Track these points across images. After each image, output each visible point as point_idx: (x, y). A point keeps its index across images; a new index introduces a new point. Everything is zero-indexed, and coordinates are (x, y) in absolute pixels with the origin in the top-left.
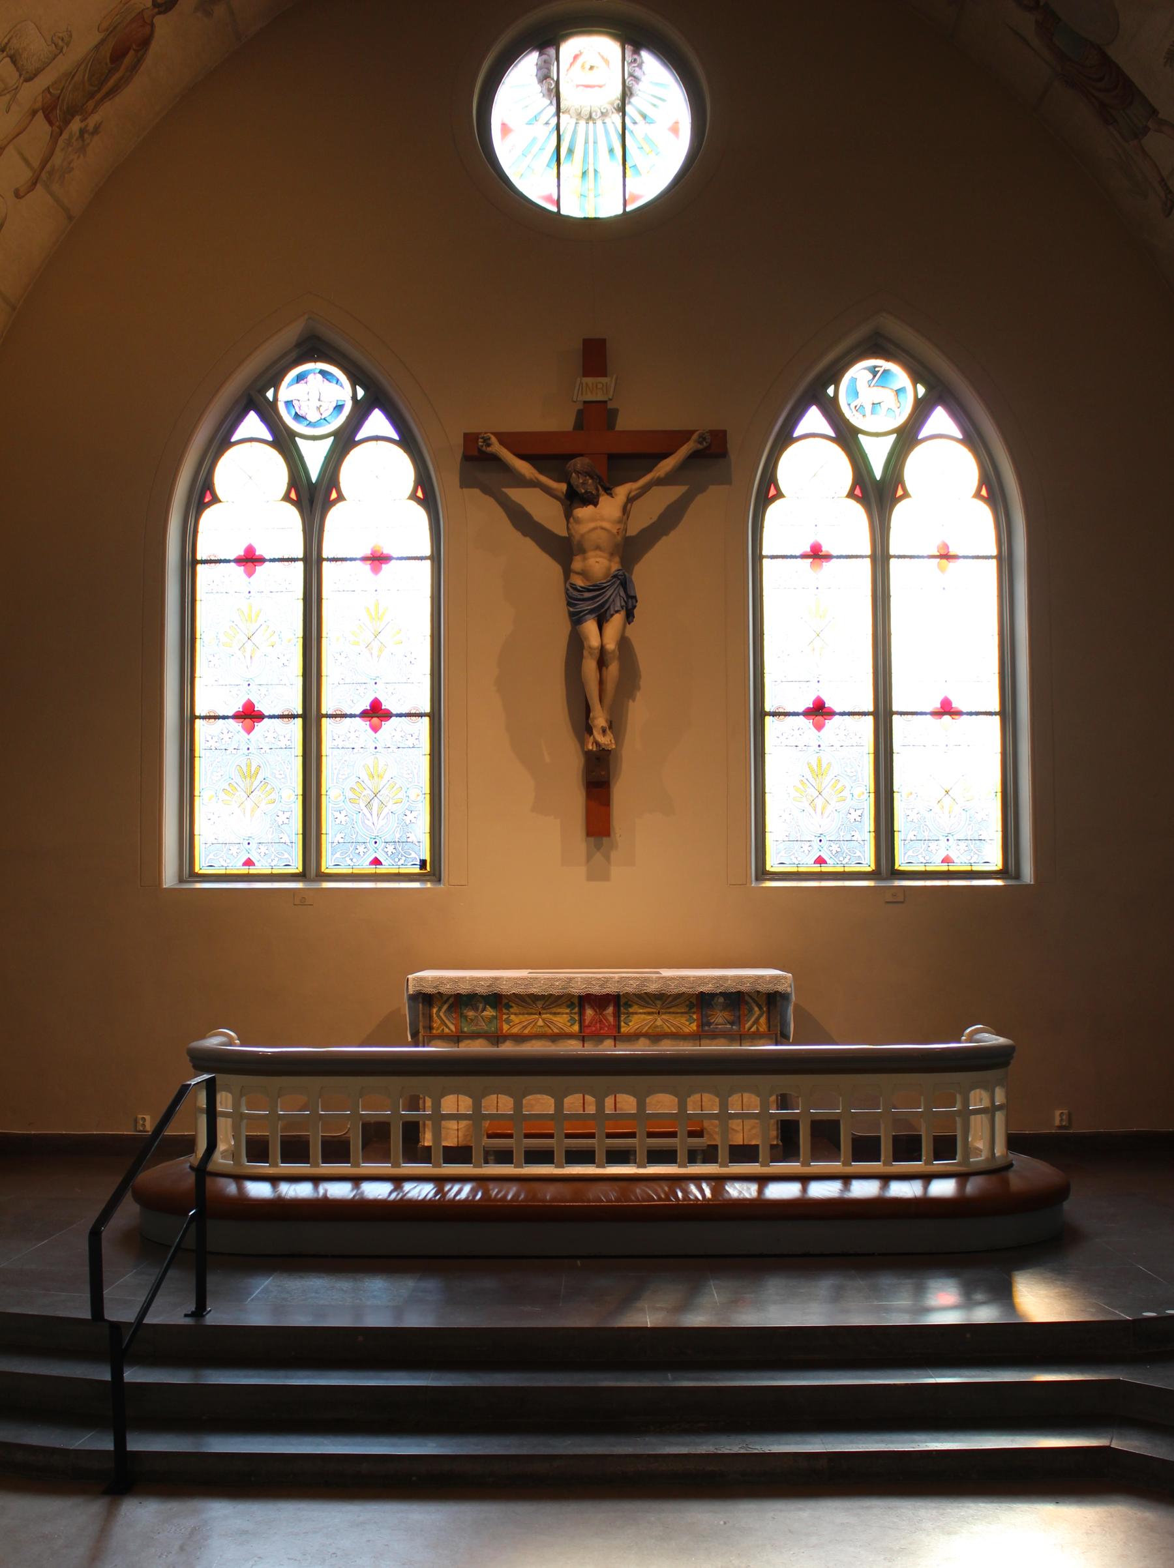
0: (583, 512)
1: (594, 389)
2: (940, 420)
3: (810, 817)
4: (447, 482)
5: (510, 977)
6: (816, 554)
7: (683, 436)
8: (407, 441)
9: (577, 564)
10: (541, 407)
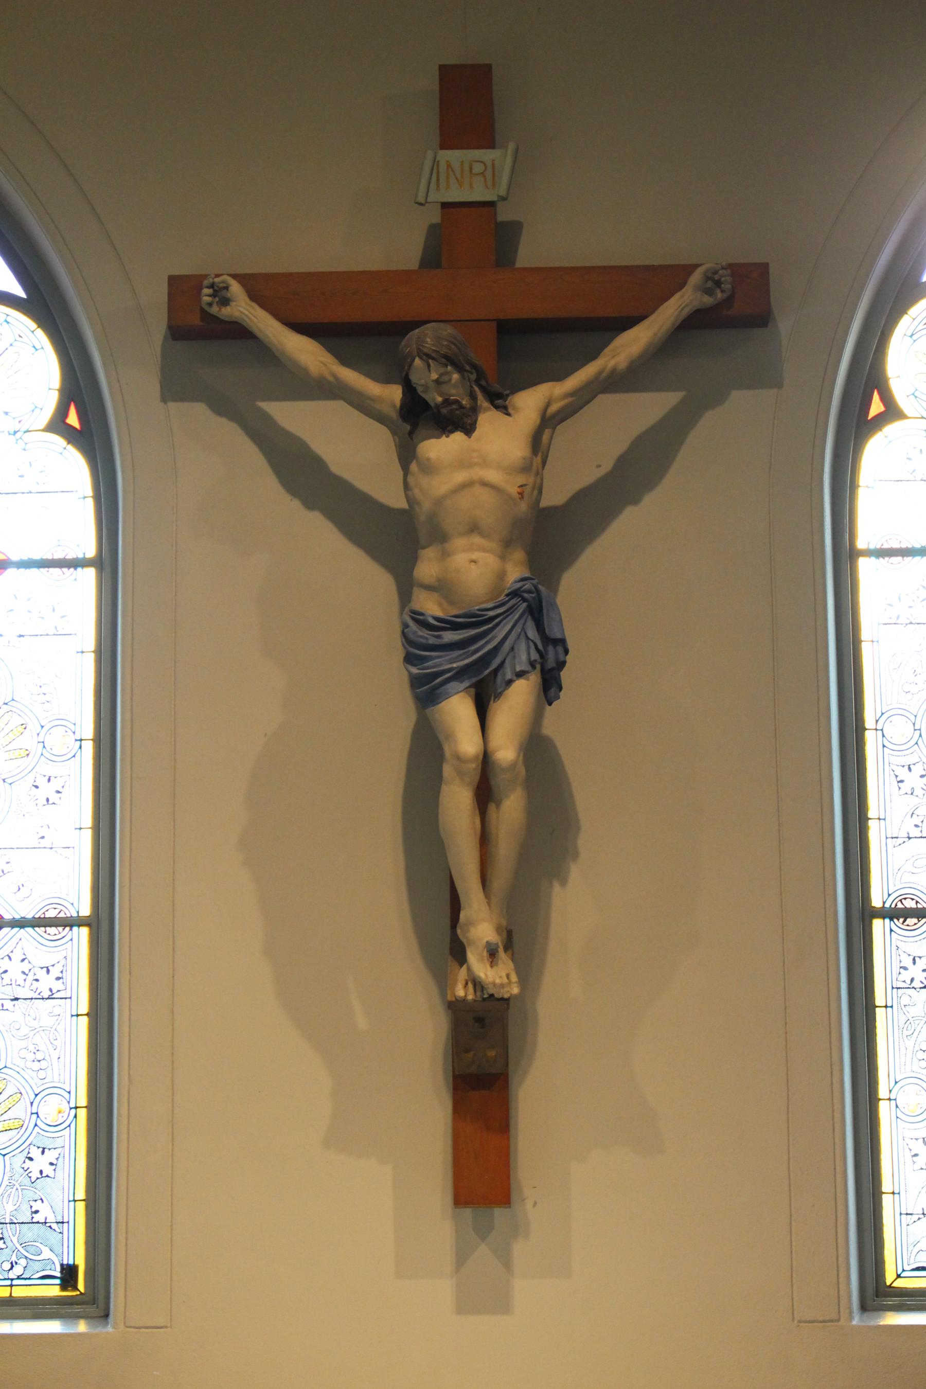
0: (440, 448)
1: (471, 176)
7: (673, 277)
9: (427, 568)
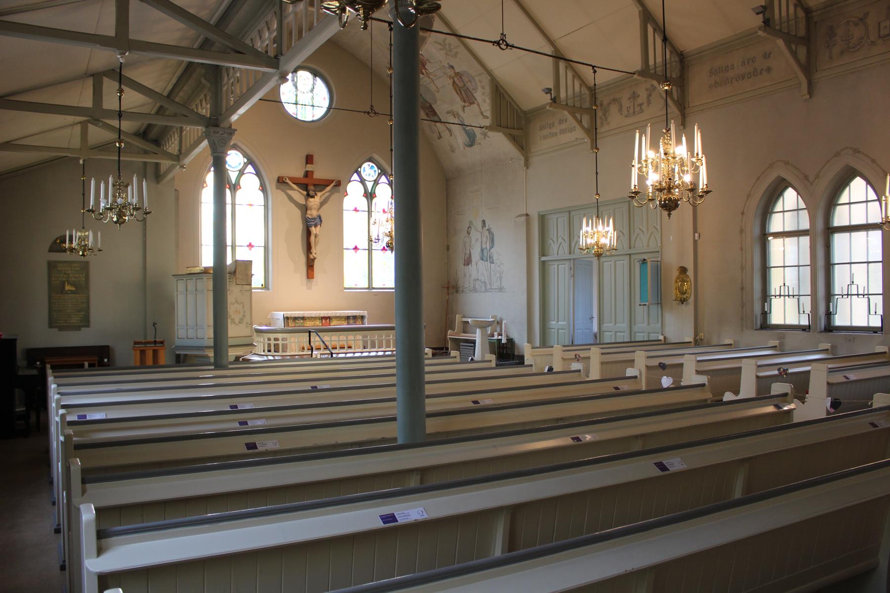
0: (311, 200)
1: (309, 168)
2: (383, 179)
3: (354, 275)
4: (271, 186)
5: (307, 314)
6: (356, 210)
7: (332, 181)
8: (258, 174)
9: (309, 212)
10: (297, 170)
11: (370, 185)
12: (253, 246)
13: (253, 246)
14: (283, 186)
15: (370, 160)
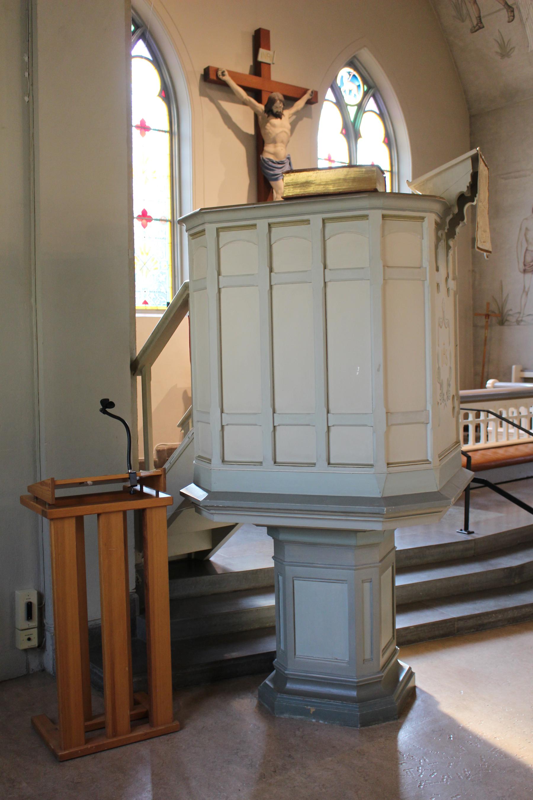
0: (275, 121)
4: (187, 89)
11: (352, 111)
12: (150, 219)
13: (150, 219)
14: (215, 93)
15: (351, 64)
